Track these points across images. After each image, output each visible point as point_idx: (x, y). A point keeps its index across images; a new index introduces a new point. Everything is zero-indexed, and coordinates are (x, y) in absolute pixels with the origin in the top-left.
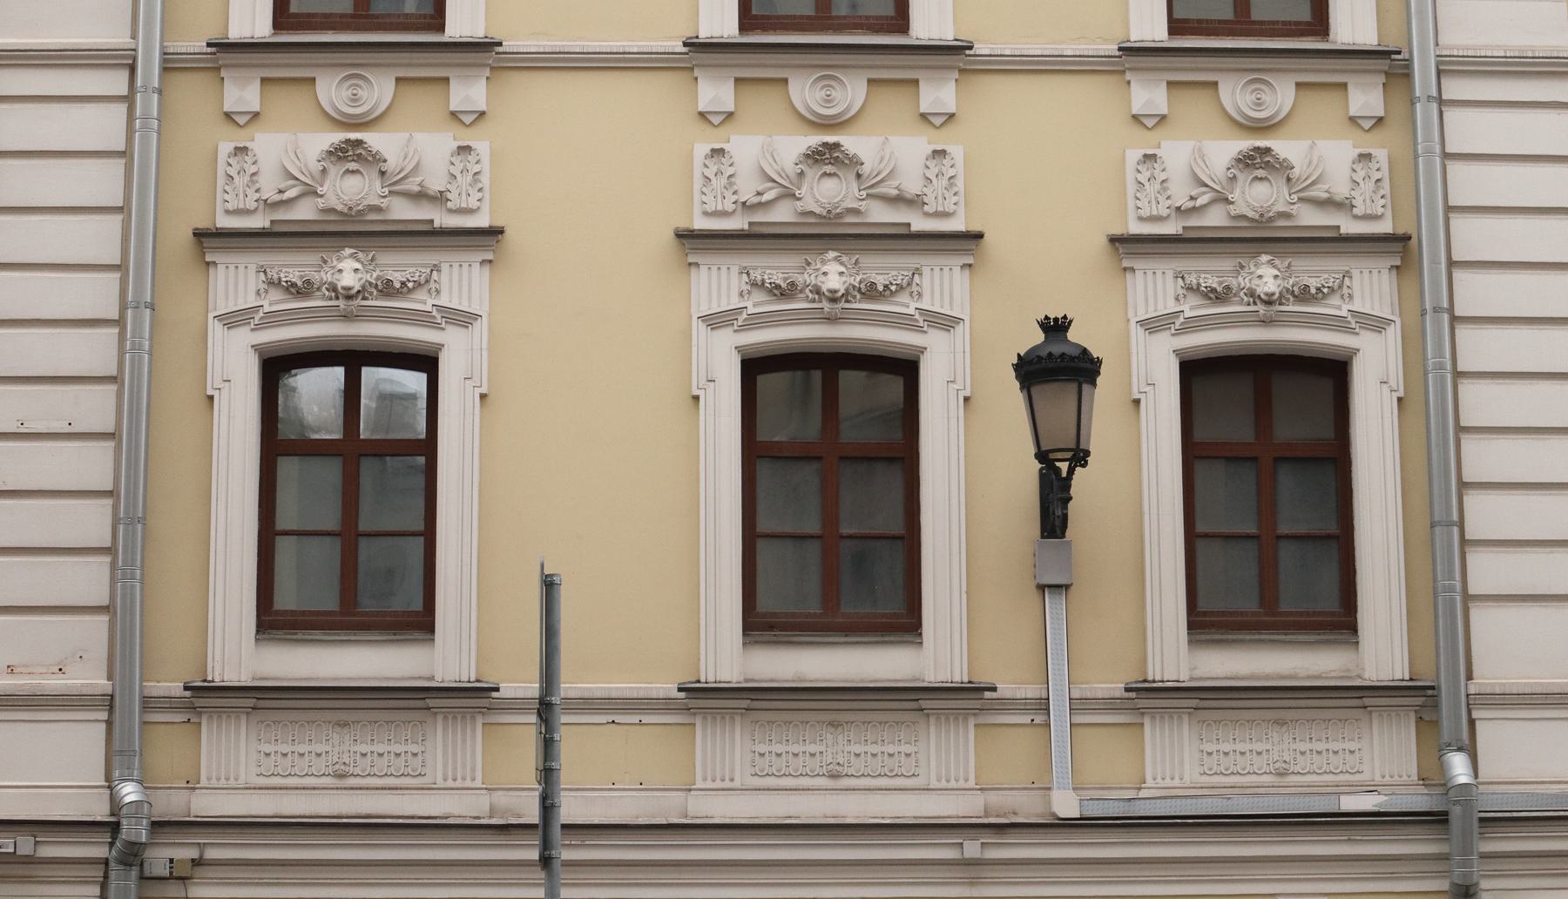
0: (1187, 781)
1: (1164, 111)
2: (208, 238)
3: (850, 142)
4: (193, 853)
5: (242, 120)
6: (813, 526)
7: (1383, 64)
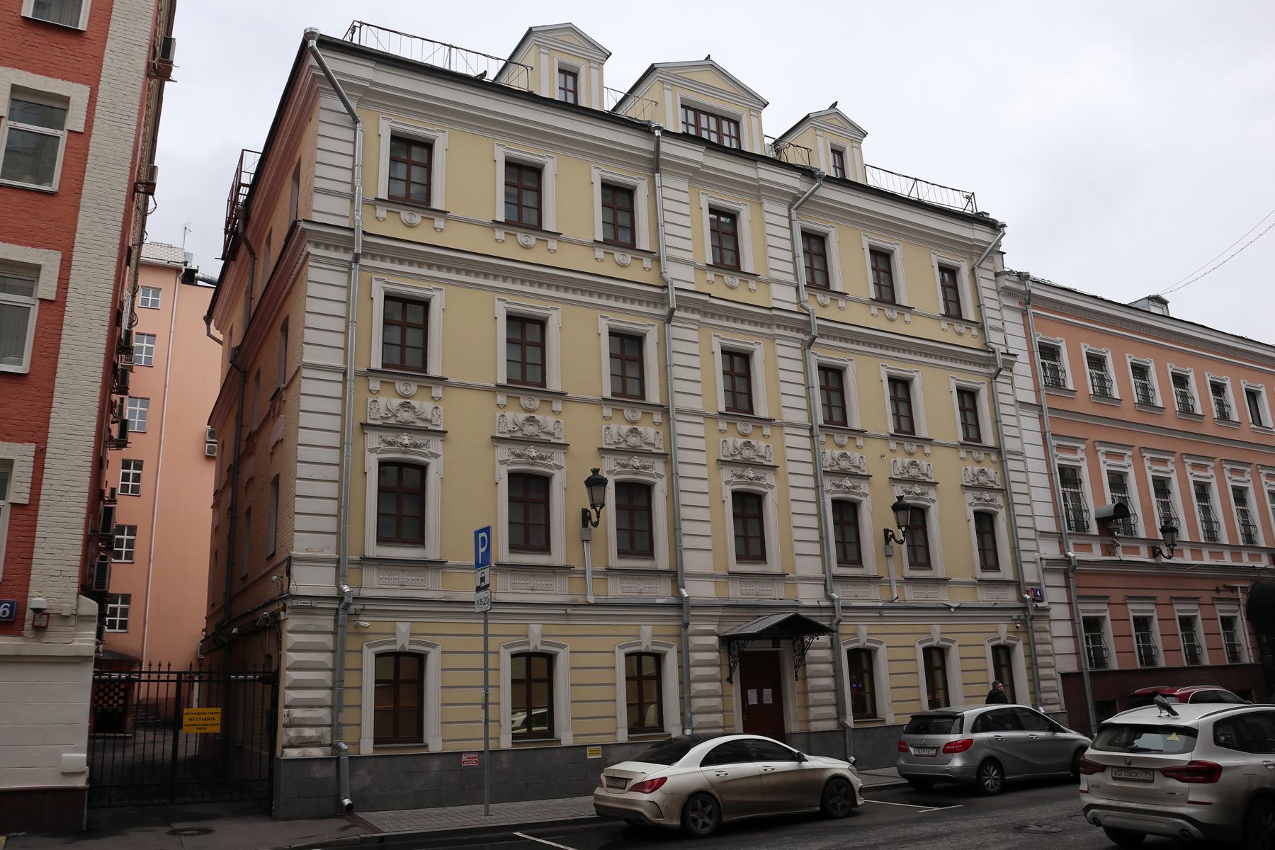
0: (618, 594)
1: (611, 416)
2: (364, 426)
3: (413, 402)
4: (361, 607)
5: (502, 407)
6: (522, 521)
7: (661, 409)
